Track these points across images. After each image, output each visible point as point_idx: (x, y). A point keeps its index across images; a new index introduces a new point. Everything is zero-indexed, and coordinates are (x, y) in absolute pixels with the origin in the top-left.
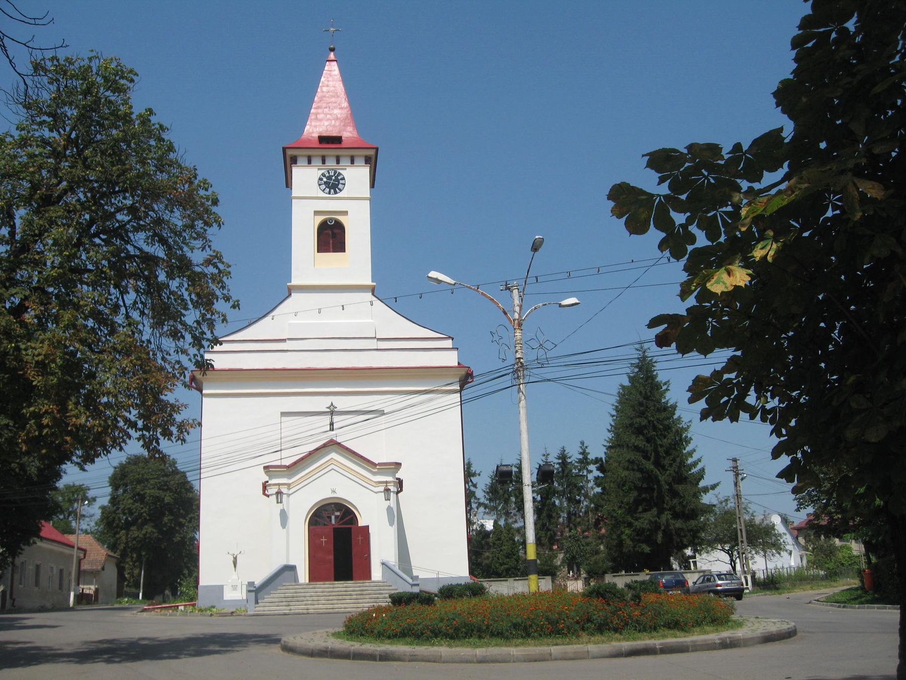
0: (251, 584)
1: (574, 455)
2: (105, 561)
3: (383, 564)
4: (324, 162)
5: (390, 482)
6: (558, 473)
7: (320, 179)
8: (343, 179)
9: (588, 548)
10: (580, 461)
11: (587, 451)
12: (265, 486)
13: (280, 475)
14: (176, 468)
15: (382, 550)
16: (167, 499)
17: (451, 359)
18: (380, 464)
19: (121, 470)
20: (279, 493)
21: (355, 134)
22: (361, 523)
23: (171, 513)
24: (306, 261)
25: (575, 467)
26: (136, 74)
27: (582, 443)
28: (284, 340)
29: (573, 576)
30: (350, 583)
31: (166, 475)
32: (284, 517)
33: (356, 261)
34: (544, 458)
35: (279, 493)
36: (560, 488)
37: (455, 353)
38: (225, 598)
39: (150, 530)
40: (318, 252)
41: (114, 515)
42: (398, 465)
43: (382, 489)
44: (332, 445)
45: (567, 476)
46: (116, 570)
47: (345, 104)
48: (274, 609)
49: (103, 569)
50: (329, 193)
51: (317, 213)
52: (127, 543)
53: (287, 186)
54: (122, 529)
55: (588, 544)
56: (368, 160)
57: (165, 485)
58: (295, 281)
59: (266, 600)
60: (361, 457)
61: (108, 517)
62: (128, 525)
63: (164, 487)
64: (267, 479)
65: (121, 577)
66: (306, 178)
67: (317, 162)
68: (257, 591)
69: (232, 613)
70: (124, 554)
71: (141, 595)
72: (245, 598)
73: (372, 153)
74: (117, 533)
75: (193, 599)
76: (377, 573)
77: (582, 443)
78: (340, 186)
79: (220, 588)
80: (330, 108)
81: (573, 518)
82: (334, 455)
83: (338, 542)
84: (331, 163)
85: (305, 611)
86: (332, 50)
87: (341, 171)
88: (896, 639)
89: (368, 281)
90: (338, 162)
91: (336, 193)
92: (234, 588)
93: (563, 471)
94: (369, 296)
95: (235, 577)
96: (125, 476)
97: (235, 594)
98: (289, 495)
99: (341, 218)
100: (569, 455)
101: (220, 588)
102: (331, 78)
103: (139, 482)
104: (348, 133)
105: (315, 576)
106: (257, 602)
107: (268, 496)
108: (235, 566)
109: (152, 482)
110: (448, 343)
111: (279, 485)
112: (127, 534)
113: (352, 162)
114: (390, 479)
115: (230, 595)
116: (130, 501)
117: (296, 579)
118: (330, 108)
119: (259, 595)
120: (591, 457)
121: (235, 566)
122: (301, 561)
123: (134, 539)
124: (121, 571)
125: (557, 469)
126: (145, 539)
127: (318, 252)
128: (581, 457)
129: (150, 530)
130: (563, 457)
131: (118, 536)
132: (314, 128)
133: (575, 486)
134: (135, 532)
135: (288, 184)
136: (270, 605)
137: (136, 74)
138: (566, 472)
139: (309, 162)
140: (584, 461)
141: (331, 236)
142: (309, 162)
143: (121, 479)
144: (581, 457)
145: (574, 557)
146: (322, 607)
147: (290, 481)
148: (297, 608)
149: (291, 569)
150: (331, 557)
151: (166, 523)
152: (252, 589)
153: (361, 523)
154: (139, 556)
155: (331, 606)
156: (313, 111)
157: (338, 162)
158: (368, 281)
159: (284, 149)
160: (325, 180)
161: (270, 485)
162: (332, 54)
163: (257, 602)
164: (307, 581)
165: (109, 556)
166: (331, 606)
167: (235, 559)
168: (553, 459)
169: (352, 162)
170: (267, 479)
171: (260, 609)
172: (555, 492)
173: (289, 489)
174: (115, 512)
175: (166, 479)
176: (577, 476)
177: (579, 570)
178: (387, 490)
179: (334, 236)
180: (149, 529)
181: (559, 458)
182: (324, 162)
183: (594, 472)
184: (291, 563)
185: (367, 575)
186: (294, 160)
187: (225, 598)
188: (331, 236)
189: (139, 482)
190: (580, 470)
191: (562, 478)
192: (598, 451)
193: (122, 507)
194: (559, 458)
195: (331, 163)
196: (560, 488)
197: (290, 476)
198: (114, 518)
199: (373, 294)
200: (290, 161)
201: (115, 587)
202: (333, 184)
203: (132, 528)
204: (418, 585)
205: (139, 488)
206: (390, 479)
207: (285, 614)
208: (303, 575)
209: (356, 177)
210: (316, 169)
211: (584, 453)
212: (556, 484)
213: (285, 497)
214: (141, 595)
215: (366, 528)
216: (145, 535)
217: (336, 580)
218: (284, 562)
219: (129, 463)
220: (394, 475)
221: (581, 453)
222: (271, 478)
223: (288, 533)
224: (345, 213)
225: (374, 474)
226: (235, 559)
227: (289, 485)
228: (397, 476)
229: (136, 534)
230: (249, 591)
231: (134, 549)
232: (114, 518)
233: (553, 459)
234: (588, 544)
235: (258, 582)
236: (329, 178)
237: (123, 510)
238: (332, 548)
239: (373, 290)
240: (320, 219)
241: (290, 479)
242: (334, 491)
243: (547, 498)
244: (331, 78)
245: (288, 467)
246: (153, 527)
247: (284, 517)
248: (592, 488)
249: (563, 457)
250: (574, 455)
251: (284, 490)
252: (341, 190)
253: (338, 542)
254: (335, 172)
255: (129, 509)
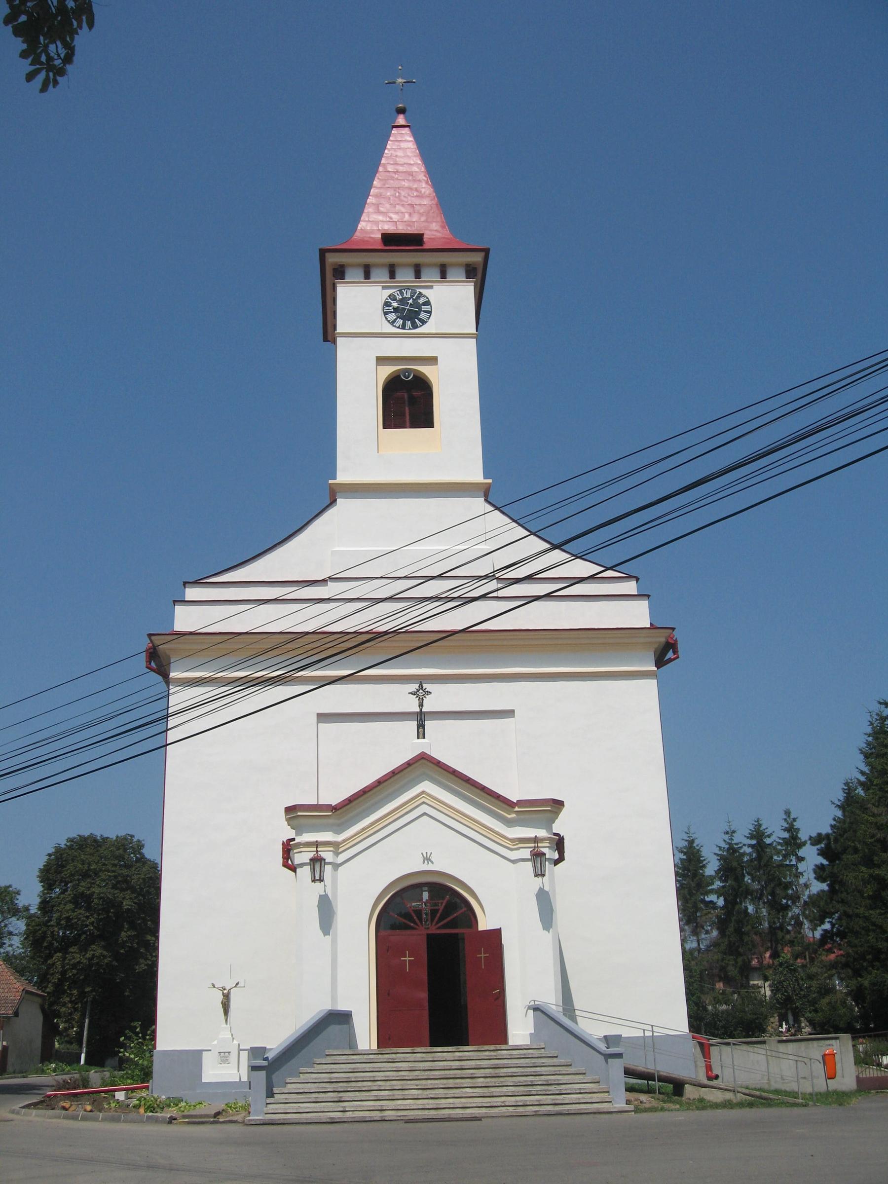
0: (256, 1052)
1: (776, 833)
2: (20, 1003)
3: (536, 1009)
4: (392, 275)
5: (543, 840)
6: (751, 860)
7: (387, 304)
8: (428, 303)
9: (814, 983)
10: (786, 842)
11: (797, 825)
12: (288, 848)
13: (316, 828)
14: (142, 855)
15: (526, 984)
16: (127, 904)
17: (638, 615)
18: (520, 803)
19: (57, 859)
20: (317, 861)
21: (446, 233)
22: (484, 924)
23: (133, 926)
24: (362, 442)
25: (778, 853)
26: (44, 89)
27: (788, 813)
28: (324, 582)
29: (788, 1030)
30: (467, 1051)
31: (127, 866)
32: (326, 911)
33: (455, 440)
34: (726, 837)
35: (317, 861)
36: (756, 886)
37: (644, 604)
38: (205, 1080)
39: (99, 951)
40: (385, 426)
41: (44, 929)
42: (558, 804)
43: (526, 853)
44: (424, 765)
45: (766, 865)
46: (41, 1018)
47: (426, 189)
48: (309, 1109)
49: (16, 1014)
50: (403, 327)
51: (382, 360)
52: (63, 973)
53: (326, 339)
54: (57, 950)
55: (810, 977)
56: (471, 272)
57: (126, 881)
58: (342, 477)
59: (291, 1088)
60: (484, 789)
61: (35, 931)
62: (65, 946)
63: (123, 884)
64: (291, 834)
65: (50, 1031)
66: (360, 304)
67: (379, 274)
68: (271, 1067)
69: (217, 1114)
70: (59, 990)
71: (83, 1056)
72: (245, 1078)
73: (478, 258)
74: (50, 956)
75: (146, 1074)
76: (520, 1029)
77: (788, 813)
78: (423, 315)
79: (195, 1057)
80: (400, 191)
81: (780, 934)
82: (427, 786)
83: (438, 964)
84: (405, 277)
85: (377, 1115)
86: (401, 111)
87: (424, 291)
88: (426, 1013)
89: (476, 474)
90: (418, 275)
91: (415, 326)
92: (224, 1057)
93: (759, 858)
94: (478, 504)
95: (226, 1035)
96: (63, 866)
97: (224, 1070)
98: (336, 866)
99: (425, 370)
100: (768, 832)
101: (195, 1057)
102: (402, 149)
103: (85, 875)
104: (434, 230)
105: (388, 1036)
106: (270, 1094)
107: (293, 869)
108: (226, 1011)
109: (103, 876)
110: (631, 587)
111: (317, 844)
112: (64, 958)
113: (443, 275)
114: (542, 833)
115: (214, 1072)
116: (70, 906)
117: (351, 1041)
118: (400, 191)
119: (274, 1077)
120: (803, 836)
121: (226, 1011)
122: (360, 999)
123: (74, 966)
124: (49, 1016)
125: (750, 854)
126: (91, 966)
127: (385, 426)
128: (786, 835)
129: (99, 951)
130: (758, 834)
131: (50, 962)
132: (376, 220)
133: (780, 883)
134: (75, 956)
135: (328, 332)
136: (301, 1098)
137: (44, 89)
138: (765, 859)
139: (367, 276)
140: (793, 842)
141: (408, 401)
142: (367, 276)
143: (58, 872)
144: (786, 835)
145: (788, 999)
146: (412, 1105)
147: (340, 838)
148: (359, 1107)
149: (342, 1018)
150: (424, 995)
151: (124, 942)
152: (261, 1062)
153: (484, 924)
154: (83, 994)
155: (431, 1103)
156: (370, 200)
157: (418, 275)
158: (476, 474)
159: (323, 253)
160: (395, 304)
161: (299, 845)
162: (401, 116)
163: (270, 1094)
164: (374, 1046)
165: (28, 992)
166: (431, 1103)
167: (227, 997)
168: (742, 838)
169: (443, 275)
170: (291, 834)
171: (276, 1109)
172: (748, 892)
173: (337, 854)
174: (46, 924)
175: (125, 872)
176: (781, 866)
177: (797, 1021)
178: (537, 855)
179: (412, 401)
180: (97, 950)
181: (752, 837)
182: (392, 275)
183: (811, 857)
184: (342, 1007)
185: (497, 1032)
186: (340, 273)
187: (205, 1080)
188: (408, 401)
189: (85, 875)
190: (785, 857)
191: (758, 868)
192: (819, 817)
193: (55, 915)
194: (752, 837)
195: (405, 277)
196: (756, 886)
197: (339, 829)
198: (45, 933)
199: (486, 500)
200: (331, 274)
201: (38, 1043)
202: (409, 313)
203: (71, 950)
204: (619, 1056)
205: (83, 886)
206: (542, 833)
207: (332, 1122)
208: (366, 1032)
209: (452, 302)
210: (378, 289)
211: (791, 829)
212: (747, 879)
213: (328, 869)
214: (83, 1056)
215: (495, 935)
216: (91, 959)
217: (435, 1042)
218: (328, 1006)
219: (70, 848)
220: (549, 828)
221: (786, 830)
222: (299, 831)
223: (334, 942)
224: (432, 360)
225: (509, 823)
226: (227, 997)
227: (336, 845)
228: (557, 827)
229: (78, 957)
230: (254, 1068)
231: (74, 983)
232: (45, 933)
233: (742, 838)
234: (810, 977)
235: (275, 1040)
236: (403, 301)
237: (59, 919)
238: (424, 976)
239: (486, 493)
240: (387, 371)
241: (338, 832)
242: (427, 859)
243: (734, 903)
244: (402, 149)
245: (335, 809)
246: (104, 948)
247: (326, 911)
248: (806, 886)
249: (758, 834)
250: (776, 833)
251: (327, 855)
252: (424, 322)
253: (438, 964)
254: (413, 293)
255: (68, 919)
